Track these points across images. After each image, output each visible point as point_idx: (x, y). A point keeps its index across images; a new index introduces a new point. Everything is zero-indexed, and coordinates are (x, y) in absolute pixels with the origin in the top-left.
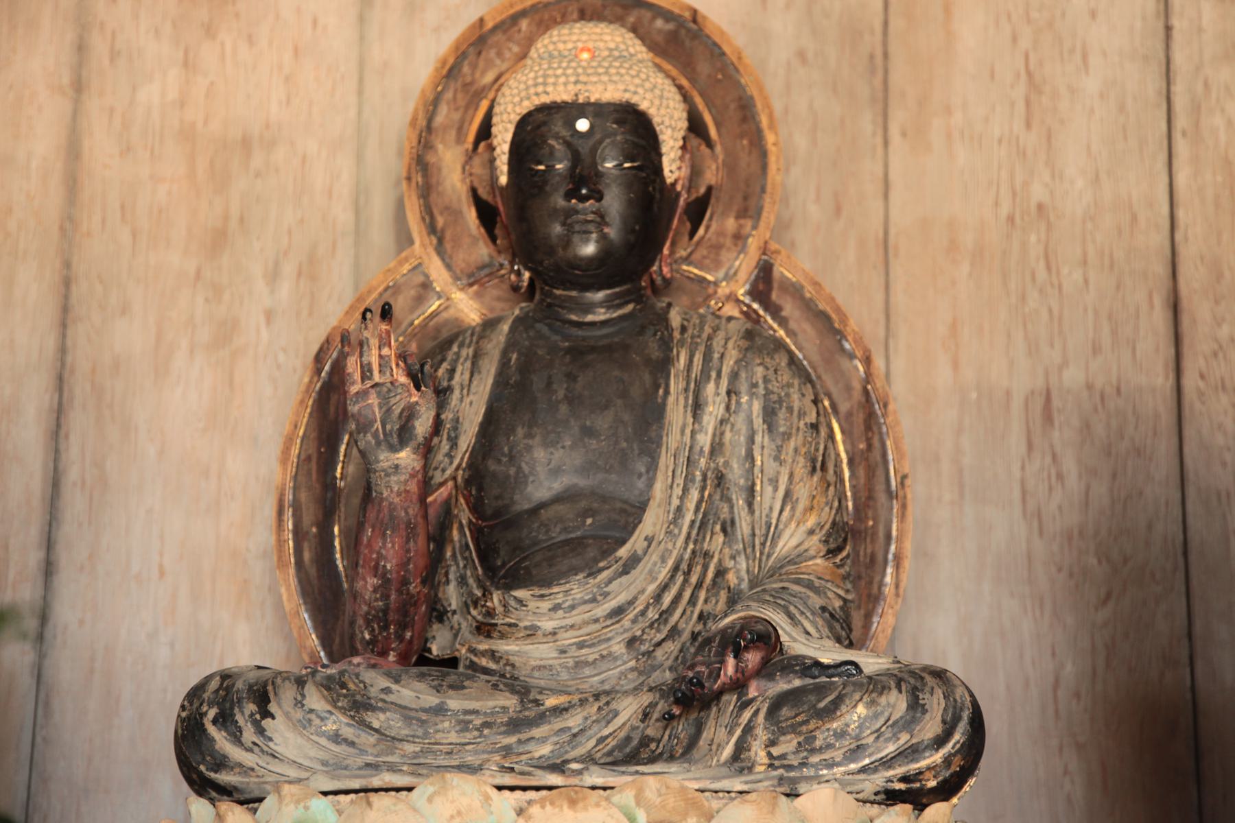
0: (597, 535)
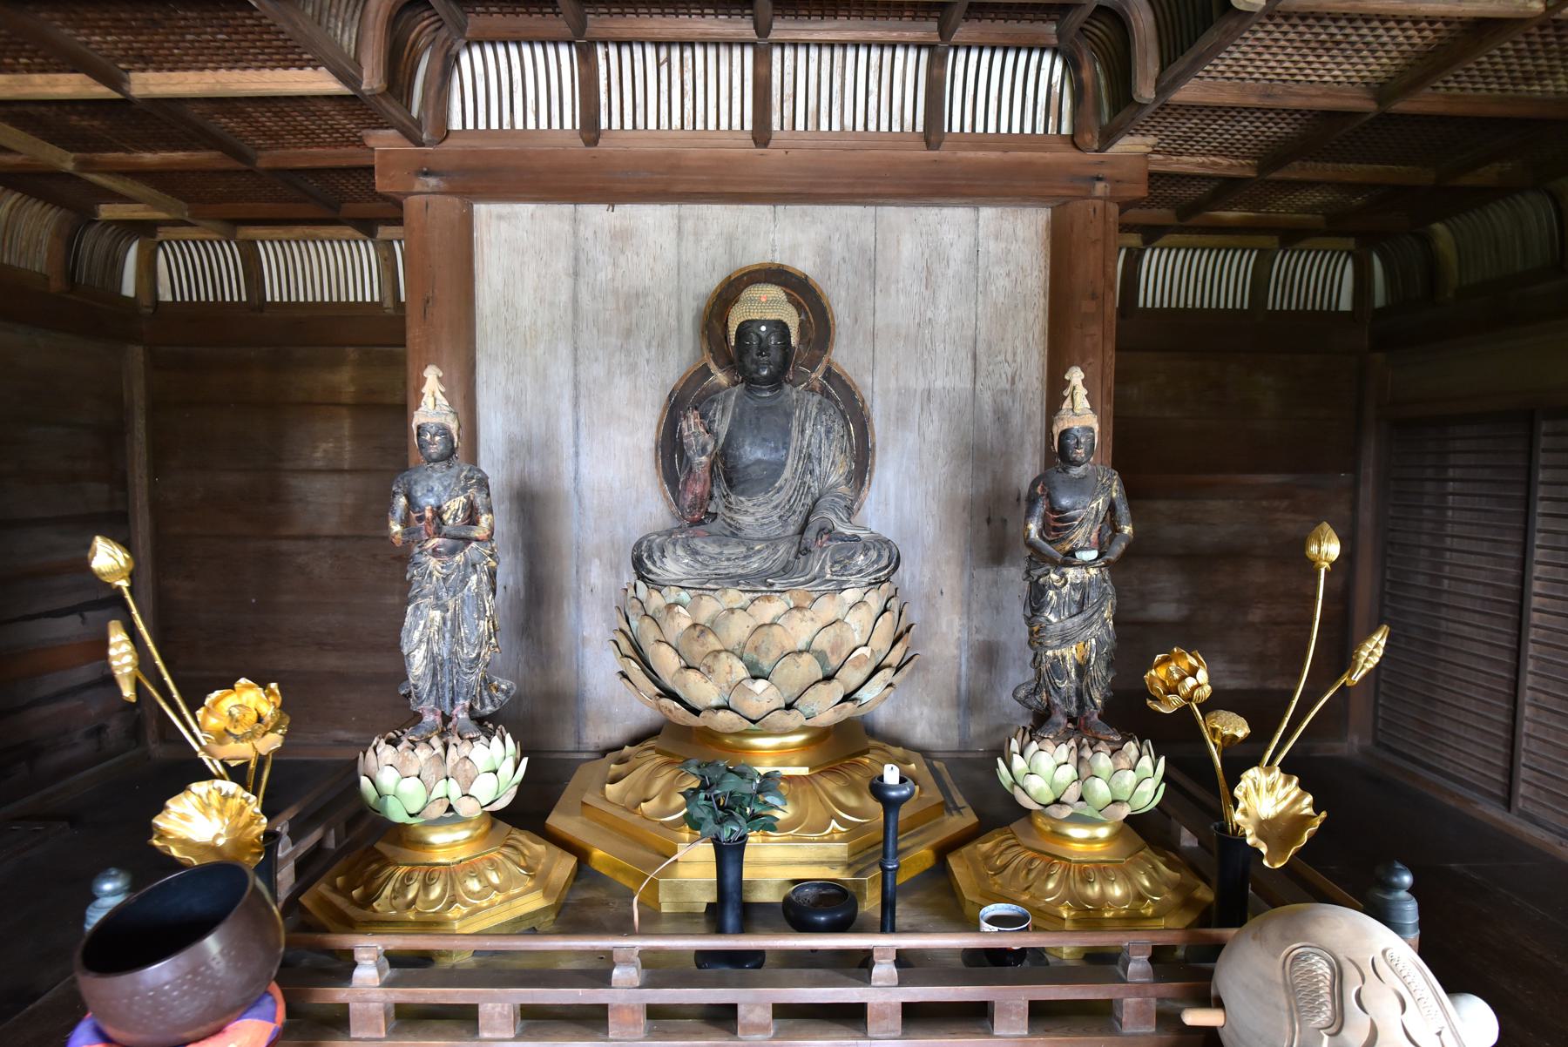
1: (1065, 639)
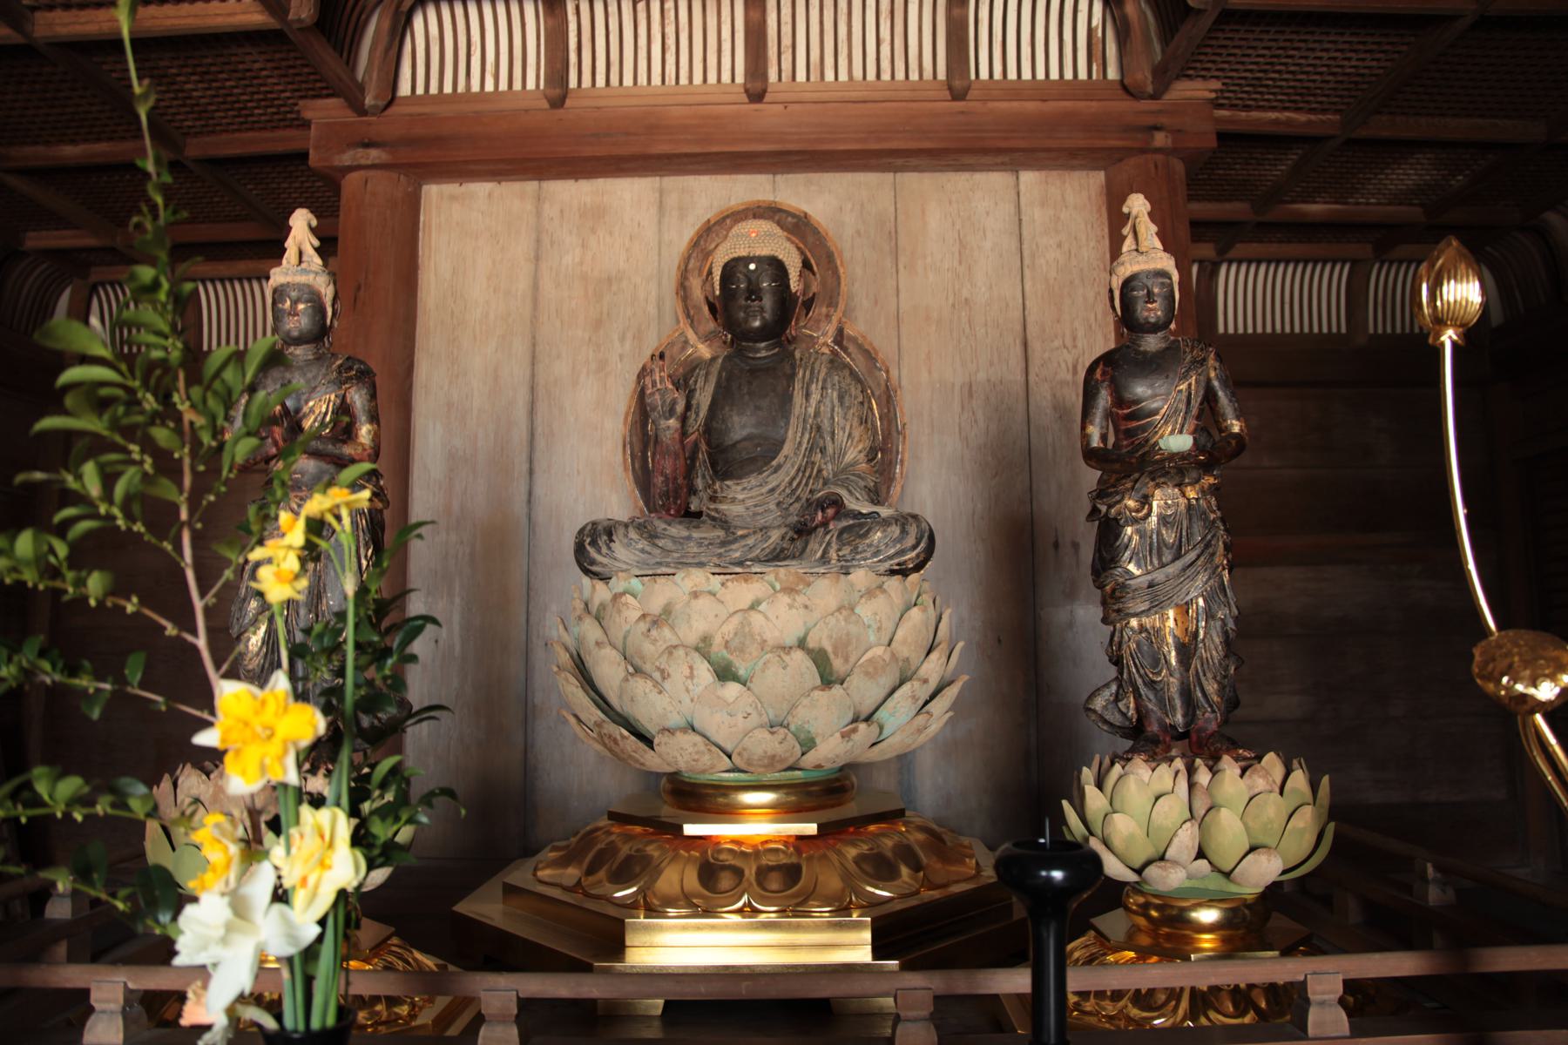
0: (763, 455)
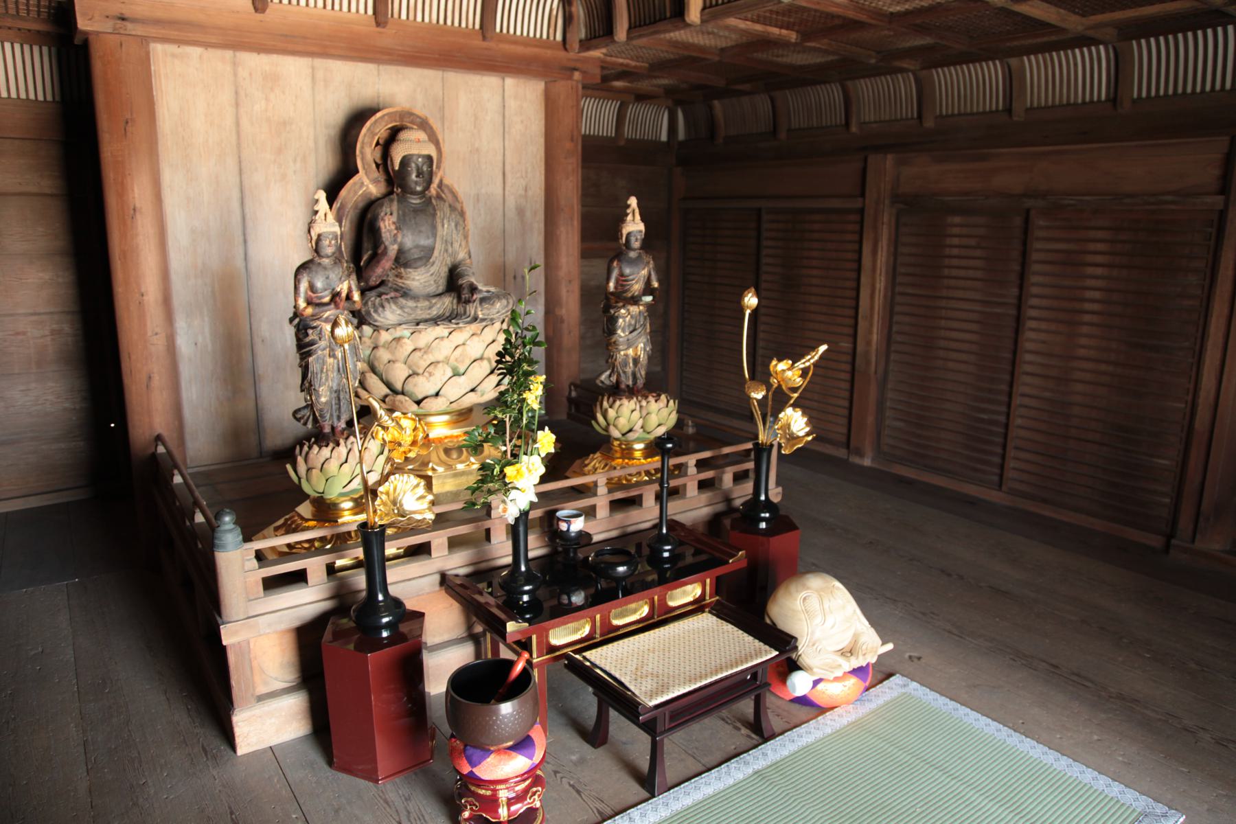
0: (426, 256)
1: (629, 344)
